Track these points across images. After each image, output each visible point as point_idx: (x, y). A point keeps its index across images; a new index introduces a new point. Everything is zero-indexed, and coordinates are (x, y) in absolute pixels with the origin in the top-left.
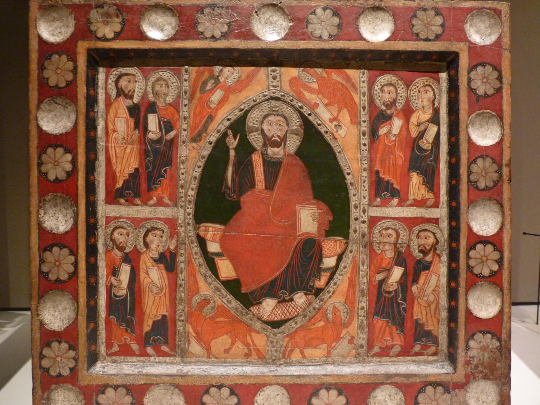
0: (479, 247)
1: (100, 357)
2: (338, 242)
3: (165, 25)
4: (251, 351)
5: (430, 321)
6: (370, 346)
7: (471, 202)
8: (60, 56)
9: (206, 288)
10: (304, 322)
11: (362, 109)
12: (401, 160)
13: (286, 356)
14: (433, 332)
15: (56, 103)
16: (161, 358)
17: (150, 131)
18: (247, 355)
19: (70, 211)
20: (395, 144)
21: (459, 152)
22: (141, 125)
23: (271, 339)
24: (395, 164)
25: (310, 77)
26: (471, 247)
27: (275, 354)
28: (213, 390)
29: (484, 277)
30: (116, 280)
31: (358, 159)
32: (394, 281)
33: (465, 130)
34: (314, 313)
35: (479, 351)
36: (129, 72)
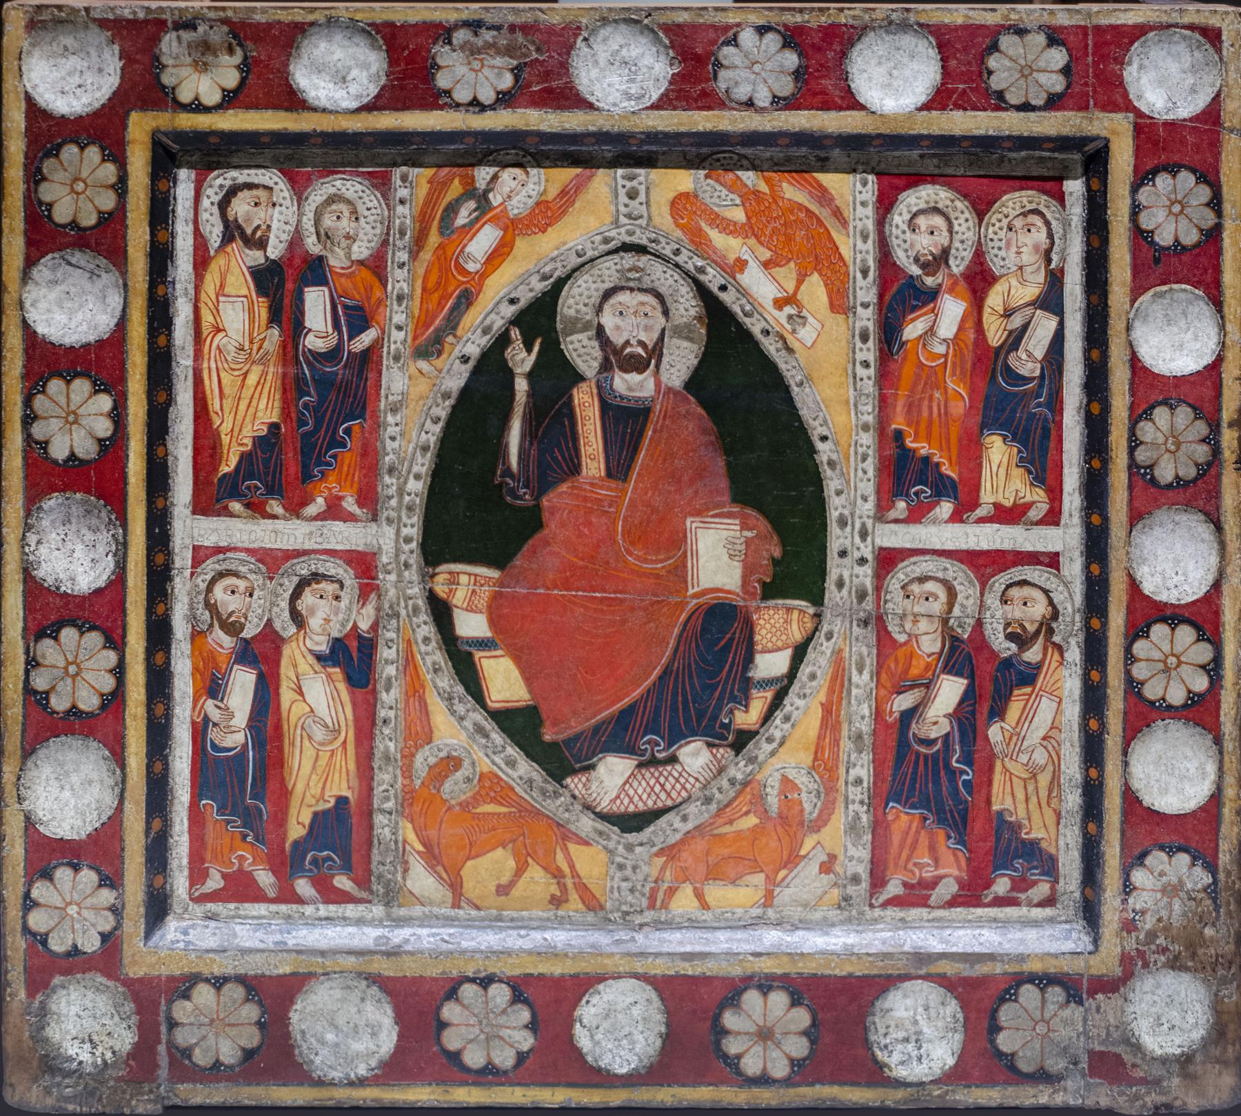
0: (1159, 631)
1: (175, 906)
2: (795, 614)
3: (350, 69)
4: (566, 890)
5: (1036, 816)
6: (878, 881)
7: (1136, 517)
8: (82, 149)
9: (453, 729)
10: (706, 815)
11: (859, 275)
12: (961, 404)
13: (658, 903)
14: (1044, 845)
15: (70, 264)
16: (332, 907)
17: (310, 330)
18: (557, 901)
19: (104, 537)
20: (946, 362)
21: (1107, 389)
22: (286, 316)
23: (619, 859)
24: (946, 413)
25: (723, 196)
26: (1137, 630)
27: (630, 898)
28: (468, 991)
29: (1170, 707)
30: (219, 708)
31: (847, 402)
32: (941, 713)
33: (1124, 336)
34: (732, 794)
35: (1159, 895)
36: (256, 181)
